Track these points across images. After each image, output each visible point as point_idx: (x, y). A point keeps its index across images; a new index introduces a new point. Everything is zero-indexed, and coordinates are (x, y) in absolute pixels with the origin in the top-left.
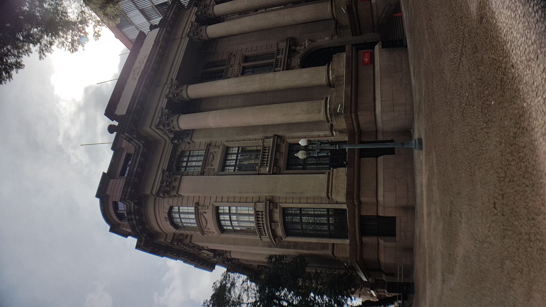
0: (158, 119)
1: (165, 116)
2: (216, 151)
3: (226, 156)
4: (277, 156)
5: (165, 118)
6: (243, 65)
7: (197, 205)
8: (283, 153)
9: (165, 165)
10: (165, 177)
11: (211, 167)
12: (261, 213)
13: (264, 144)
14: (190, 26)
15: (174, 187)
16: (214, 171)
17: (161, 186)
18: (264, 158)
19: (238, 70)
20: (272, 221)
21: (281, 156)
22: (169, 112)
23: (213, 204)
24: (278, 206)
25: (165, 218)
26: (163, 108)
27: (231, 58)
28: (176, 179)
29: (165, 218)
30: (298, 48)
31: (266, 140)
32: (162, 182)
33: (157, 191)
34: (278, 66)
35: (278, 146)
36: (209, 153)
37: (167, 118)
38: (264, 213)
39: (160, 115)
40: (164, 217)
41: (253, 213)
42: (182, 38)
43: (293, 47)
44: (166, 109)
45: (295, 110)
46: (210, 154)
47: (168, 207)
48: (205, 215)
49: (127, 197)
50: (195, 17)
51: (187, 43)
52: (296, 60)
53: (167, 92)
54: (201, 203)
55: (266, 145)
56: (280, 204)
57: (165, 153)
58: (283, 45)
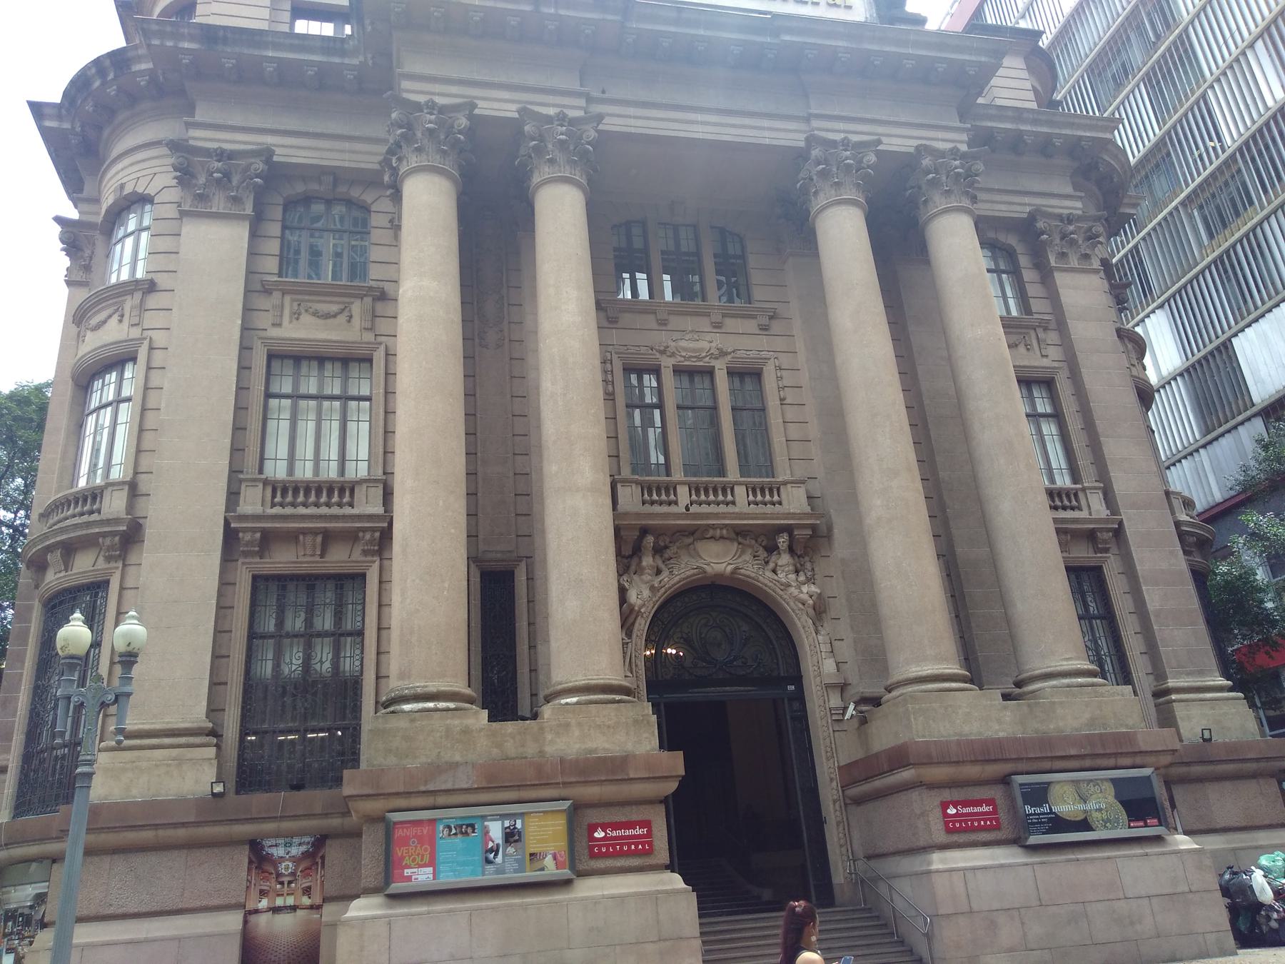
0: (842, 136)
1: (962, 166)
2: (353, 320)
4: (309, 539)
5: (956, 168)
7: (149, 287)
8: (322, 556)
9: (291, 151)
10: (243, 162)
13: (364, 486)
17: (207, 152)
18: (771, 491)
19: (694, 350)
21: (308, 552)
22: (869, 167)
24: (369, 558)
25: (122, 187)
28: (236, 200)
29: (122, 187)
30: (785, 559)
32: (221, 155)
33: (1044, 208)
35: (351, 536)
36: (1023, 331)
39: (440, 101)
40: (123, 181)
42: (807, 119)
43: (783, 540)
44: (879, 154)
45: (417, 581)
46: (1021, 333)
47: (151, 191)
48: (116, 318)
49: (156, 42)
51: (782, 143)
52: (1083, 554)
53: (831, 136)
54: (153, 301)
55: (360, 493)
56: (377, 563)
58: (794, 502)
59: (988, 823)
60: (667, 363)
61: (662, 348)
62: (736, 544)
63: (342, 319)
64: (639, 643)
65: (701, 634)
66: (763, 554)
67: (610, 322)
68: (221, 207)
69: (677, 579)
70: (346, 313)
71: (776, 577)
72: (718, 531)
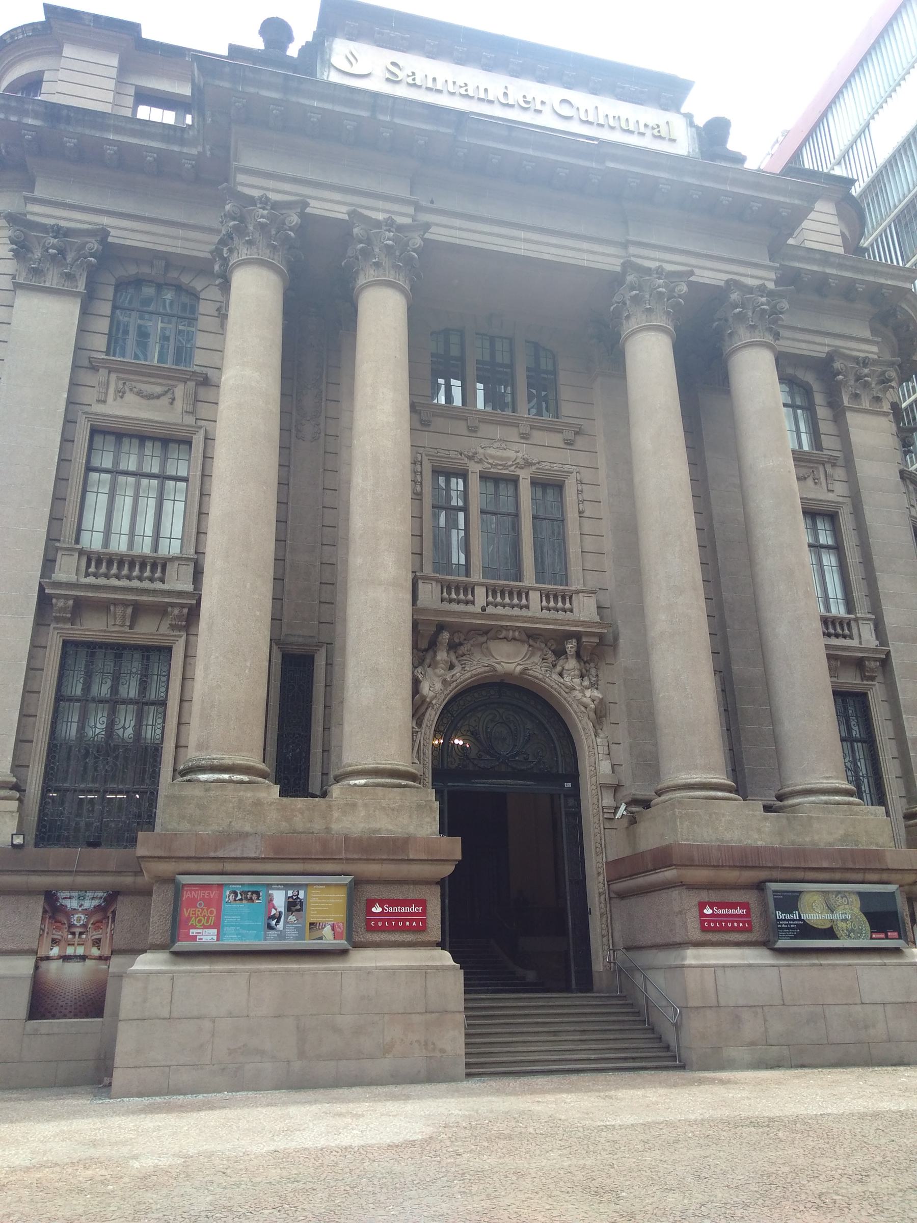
0: (657, 264)
1: (768, 303)
2: (176, 402)
3: (154, 439)
5: (659, 287)
6: (525, 477)
8: (131, 627)
11: (111, 390)
12: (158, 574)
14: (669, 267)
15: (37, 272)
16: (98, 401)
17: (44, 228)
19: (501, 459)
20: (138, 610)
22: (680, 296)
23: (200, 427)
26: (692, 273)
27: (560, 431)
28: (69, 277)
31: (191, 569)
32: (58, 231)
34: (827, 629)
36: (170, 382)
37: (660, 293)
38: (524, 612)
41: (160, 552)
42: (625, 245)
45: (221, 658)
50: (722, 284)
56: (184, 638)
57: (181, 232)
59: (741, 925)
60: (474, 469)
61: (470, 454)
62: (526, 646)
63: (165, 400)
64: (428, 734)
65: (487, 728)
66: (551, 657)
67: (422, 424)
68: (55, 282)
69: (468, 675)
70: (169, 395)
71: (562, 680)
72: (511, 632)
